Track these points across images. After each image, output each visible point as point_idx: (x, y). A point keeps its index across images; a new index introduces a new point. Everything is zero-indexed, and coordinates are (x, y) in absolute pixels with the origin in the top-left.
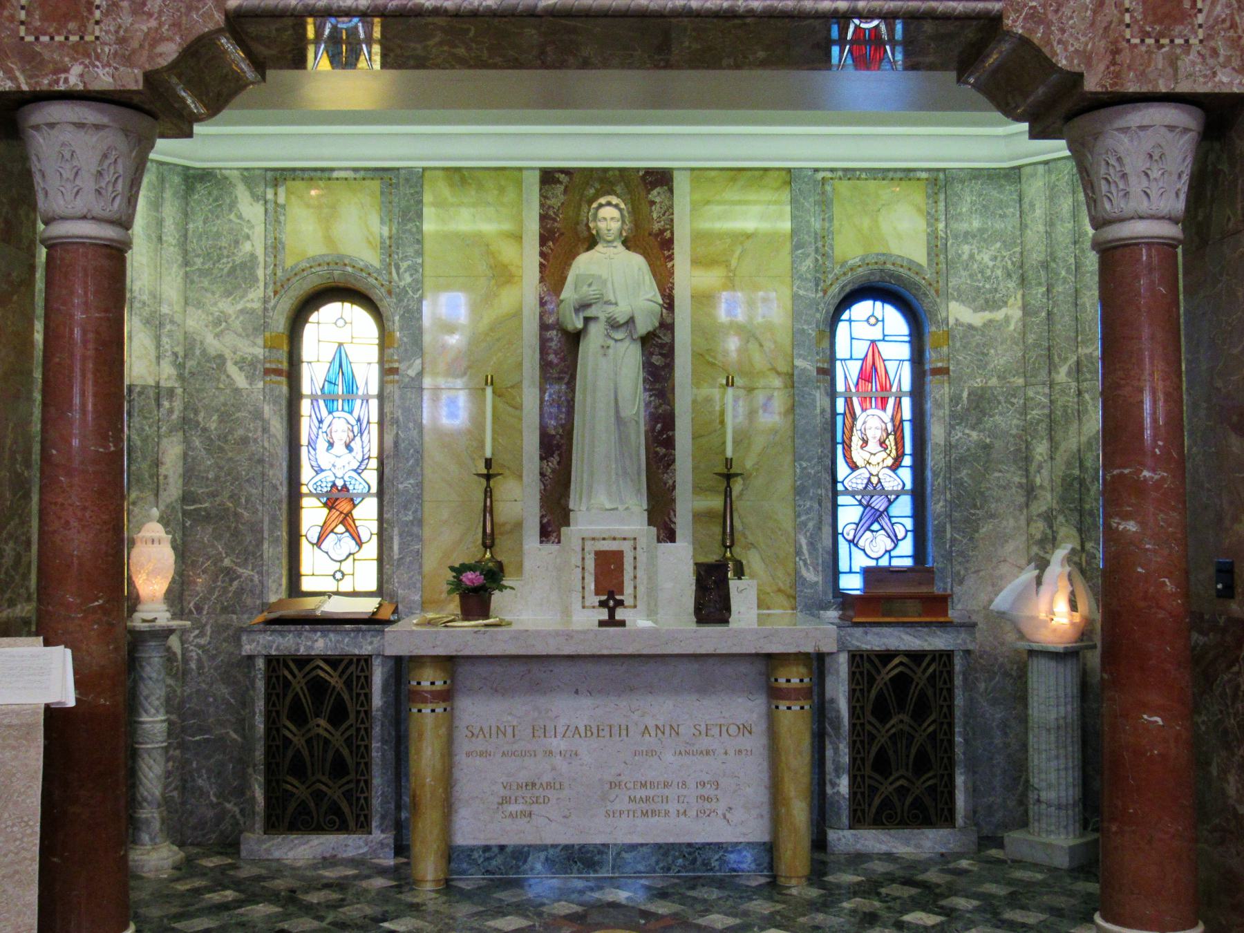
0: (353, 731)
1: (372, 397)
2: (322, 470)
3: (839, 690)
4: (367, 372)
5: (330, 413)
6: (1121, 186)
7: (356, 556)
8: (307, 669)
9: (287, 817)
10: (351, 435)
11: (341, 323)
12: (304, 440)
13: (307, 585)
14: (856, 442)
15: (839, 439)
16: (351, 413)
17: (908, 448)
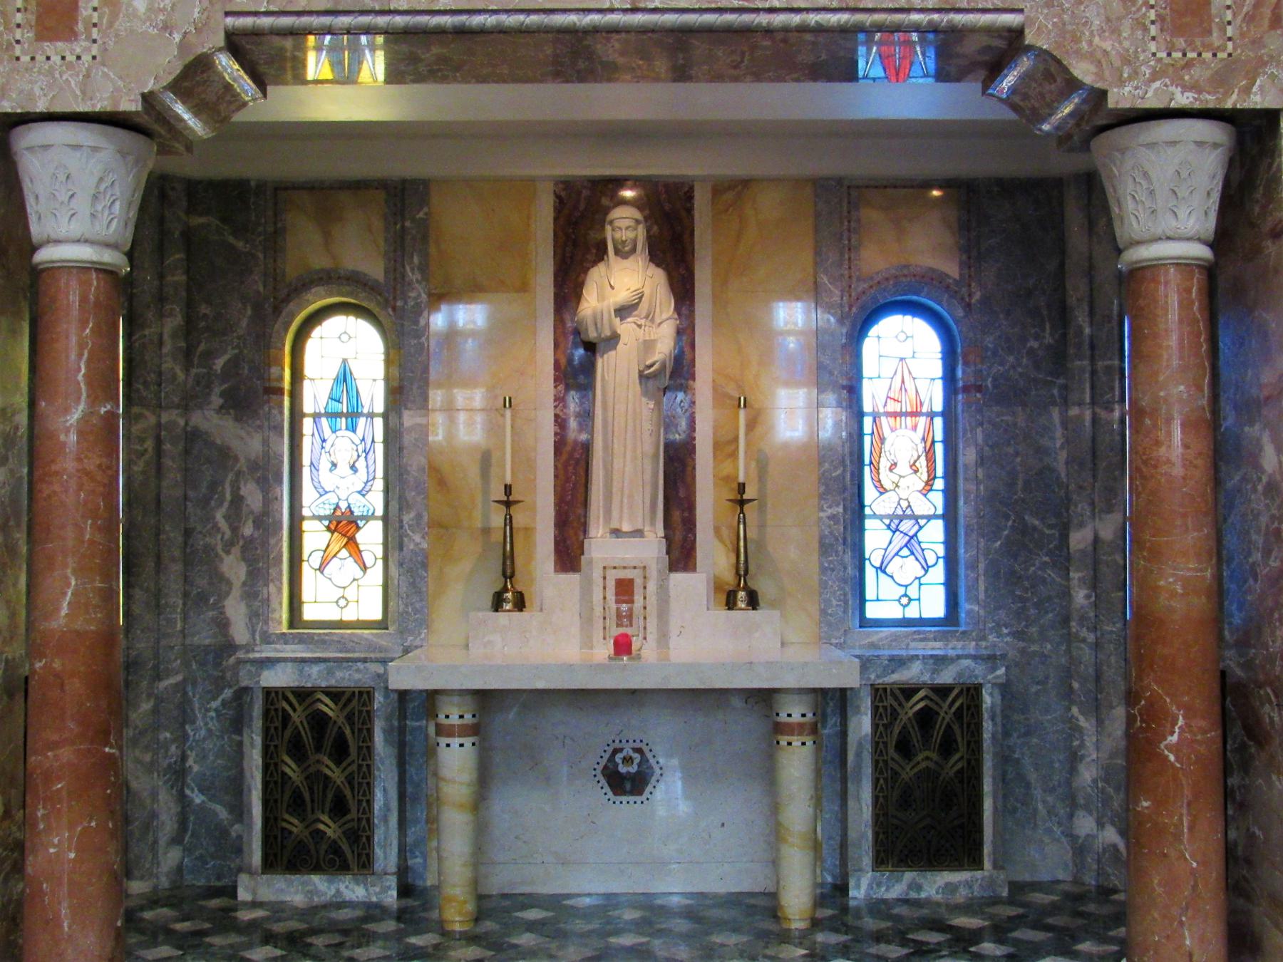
0: (354, 767)
1: (378, 415)
2: (886, 491)
3: (862, 724)
4: (372, 390)
5: (334, 432)
6: (1148, 204)
7: (360, 582)
8: (309, 701)
9: (285, 855)
10: (355, 454)
11: (345, 337)
12: (306, 460)
13: (309, 613)
14: (884, 464)
15: (867, 461)
16: (354, 431)
17: (940, 471)
